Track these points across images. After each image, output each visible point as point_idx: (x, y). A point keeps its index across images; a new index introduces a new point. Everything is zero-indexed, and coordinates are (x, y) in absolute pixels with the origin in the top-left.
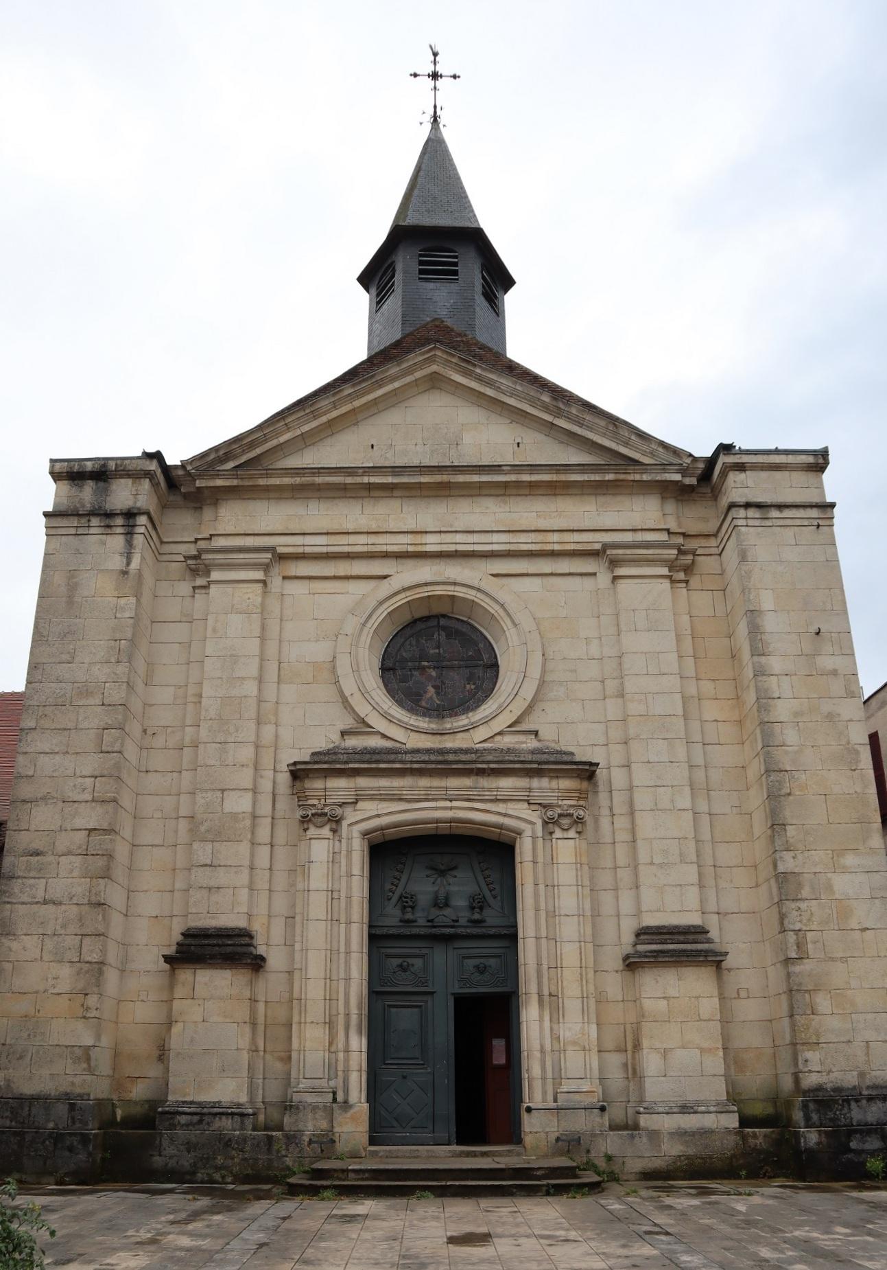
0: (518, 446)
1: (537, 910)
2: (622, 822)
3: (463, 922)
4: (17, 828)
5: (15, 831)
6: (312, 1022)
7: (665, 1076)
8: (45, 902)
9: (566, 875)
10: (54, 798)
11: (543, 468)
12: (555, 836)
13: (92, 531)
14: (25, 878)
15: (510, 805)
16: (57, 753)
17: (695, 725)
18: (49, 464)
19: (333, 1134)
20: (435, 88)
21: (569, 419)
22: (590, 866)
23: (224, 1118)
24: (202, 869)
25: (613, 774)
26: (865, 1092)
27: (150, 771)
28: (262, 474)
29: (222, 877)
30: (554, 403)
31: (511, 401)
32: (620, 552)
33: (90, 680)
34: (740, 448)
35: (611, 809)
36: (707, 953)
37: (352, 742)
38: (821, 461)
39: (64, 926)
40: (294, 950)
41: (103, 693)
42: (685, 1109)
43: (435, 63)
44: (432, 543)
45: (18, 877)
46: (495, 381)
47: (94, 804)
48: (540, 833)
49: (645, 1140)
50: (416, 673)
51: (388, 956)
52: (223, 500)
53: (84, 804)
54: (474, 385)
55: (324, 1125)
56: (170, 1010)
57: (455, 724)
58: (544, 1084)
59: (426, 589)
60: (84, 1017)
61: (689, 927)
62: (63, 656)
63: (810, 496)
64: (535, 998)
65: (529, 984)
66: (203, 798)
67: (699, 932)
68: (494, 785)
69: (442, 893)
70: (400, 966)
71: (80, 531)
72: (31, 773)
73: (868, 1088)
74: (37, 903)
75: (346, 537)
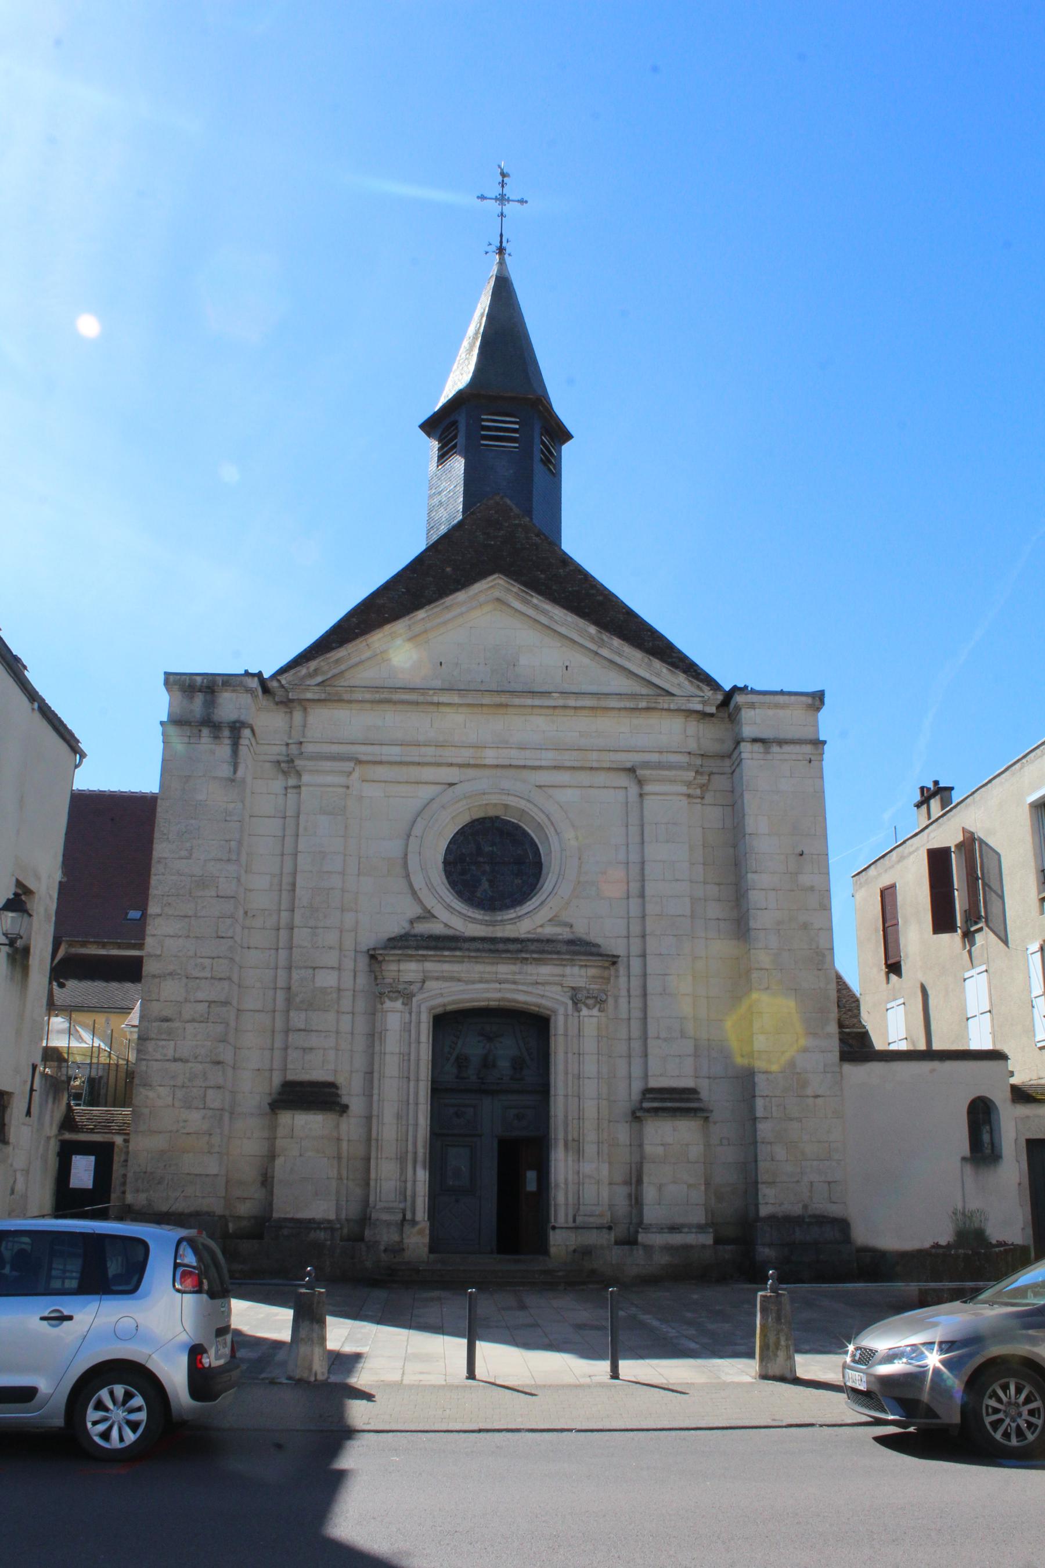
0: (567, 669)
1: (566, 1073)
6: (387, 1158)
8: (175, 1060)
10: (179, 974)
14: (157, 1039)
15: (547, 988)
16: (180, 936)
18: (163, 676)
26: (807, 1220)
29: (314, 1041)
30: (599, 635)
31: (562, 630)
34: (751, 688)
35: (629, 991)
38: (817, 703)
41: (217, 887)
43: (503, 184)
46: (548, 612)
47: (213, 981)
48: (570, 1012)
50: (473, 868)
53: (204, 980)
54: (531, 612)
55: (396, 1238)
58: (567, 1209)
63: (807, 733)
66: (298, 974)
67: (693, 1091)
72: (159, 953)
73: (810, 1216)
74: (168, 1060)
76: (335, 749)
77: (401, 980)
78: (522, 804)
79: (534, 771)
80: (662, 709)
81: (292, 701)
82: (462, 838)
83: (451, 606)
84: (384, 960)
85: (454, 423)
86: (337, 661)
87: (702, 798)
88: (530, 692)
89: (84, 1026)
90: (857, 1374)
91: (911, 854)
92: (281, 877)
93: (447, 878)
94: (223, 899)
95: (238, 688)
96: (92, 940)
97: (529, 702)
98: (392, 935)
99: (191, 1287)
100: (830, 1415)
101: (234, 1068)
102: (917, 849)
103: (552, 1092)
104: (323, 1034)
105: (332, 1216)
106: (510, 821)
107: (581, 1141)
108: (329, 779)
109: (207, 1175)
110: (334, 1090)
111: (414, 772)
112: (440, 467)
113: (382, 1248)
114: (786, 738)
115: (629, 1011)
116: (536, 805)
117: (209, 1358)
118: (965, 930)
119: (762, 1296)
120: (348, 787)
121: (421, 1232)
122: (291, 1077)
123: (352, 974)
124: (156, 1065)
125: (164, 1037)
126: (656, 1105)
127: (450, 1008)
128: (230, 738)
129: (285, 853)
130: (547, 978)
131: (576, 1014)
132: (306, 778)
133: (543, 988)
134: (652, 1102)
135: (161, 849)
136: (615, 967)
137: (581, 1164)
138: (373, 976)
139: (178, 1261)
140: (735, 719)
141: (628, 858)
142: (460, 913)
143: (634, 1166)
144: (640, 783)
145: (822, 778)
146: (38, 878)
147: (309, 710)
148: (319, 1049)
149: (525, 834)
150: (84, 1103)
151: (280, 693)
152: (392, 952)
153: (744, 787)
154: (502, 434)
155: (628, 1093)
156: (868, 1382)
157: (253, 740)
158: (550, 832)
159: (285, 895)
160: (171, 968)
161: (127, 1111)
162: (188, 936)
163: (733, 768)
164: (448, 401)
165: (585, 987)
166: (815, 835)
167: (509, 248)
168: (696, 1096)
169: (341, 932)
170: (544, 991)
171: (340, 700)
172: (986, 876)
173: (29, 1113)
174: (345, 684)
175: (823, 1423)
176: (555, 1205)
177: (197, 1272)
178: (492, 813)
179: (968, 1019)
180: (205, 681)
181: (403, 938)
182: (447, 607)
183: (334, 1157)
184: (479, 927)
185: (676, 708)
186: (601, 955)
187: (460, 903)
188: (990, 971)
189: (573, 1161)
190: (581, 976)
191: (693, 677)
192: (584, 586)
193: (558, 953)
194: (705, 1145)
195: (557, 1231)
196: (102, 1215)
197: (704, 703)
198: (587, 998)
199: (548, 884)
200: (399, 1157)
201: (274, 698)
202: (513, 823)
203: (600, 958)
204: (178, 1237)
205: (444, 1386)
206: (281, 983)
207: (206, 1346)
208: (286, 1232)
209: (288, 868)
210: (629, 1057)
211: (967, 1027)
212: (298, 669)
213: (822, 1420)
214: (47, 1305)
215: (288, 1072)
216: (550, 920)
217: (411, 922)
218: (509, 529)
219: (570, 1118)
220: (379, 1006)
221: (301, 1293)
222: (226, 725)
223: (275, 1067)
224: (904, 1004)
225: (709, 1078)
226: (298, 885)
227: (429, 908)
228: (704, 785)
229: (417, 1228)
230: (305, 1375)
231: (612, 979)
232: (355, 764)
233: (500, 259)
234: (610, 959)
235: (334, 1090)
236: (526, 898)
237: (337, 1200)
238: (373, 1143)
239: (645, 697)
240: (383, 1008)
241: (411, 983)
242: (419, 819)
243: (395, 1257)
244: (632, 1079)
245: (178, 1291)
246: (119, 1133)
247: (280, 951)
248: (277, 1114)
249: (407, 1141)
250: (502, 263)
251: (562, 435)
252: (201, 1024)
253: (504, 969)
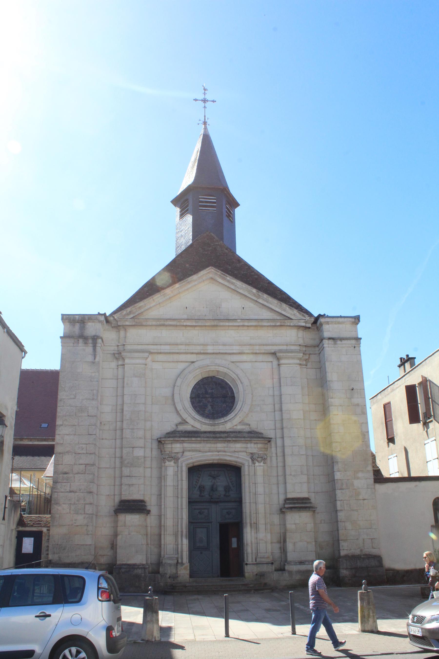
0: (243, 309)
1: (250, 492)
4: (58, 464)
5: (57, 464)
6: (169, 534)
7: (294, 551)
8: (70, 492)
10: (71, 452)
11: (253, 320)
14: (62, 482)
15: (240, 453)
16: (72, 435)
19: (177, 574)
20: (205, 107)
26: (362, 557)
27: (104, 439)
28: (144, 321)
31: (241, 291)
33: (82, 406)
34: (327, 315)
35: (276, 454)
36: (309, 507)
38: (357, 321)
39: (78, 501)
41: (88, 411)
43: (205, 94)
45: (59, 482)
47: (87, 455)
50: (204, 400)
51: (195, 509)
55: (174, 571)
63: (353, 335)
64: (249, 525)
67: (308, 499)
72: (62, 442)
73: (364, 555)
74: (67, 492)
76: (140, 347)
77: (173, 452)
78: (225, 370)
79: (230, 355)
80: (287, 326)
81: (119, 326)
82: (198, 386)
83: (191, 281)
84: (165, 443)
85: (187, 200)
86: (140, 308)
87: (306, 365)
88: (227, 319)
89: (25, 477)
90: (416, 628)
91: (397, 388)
92: (117, 406)
93: (192, 405)
94: (91, 417)
95: (95, 321)
96: (26, 437)
97: (227, 324)
98: (168, 432)
99: (105, 598)
100: (399, 649)
101: (97, 495)
102: (400, 386)
103: (243, 501)
104: (138, 478)
105: (144, 562)
106: (220, 378)
107: (257, 523)
108: (137, 361)
109: (86, 545)
110: (144, 503)
111: (176, 357)
112: (181, 220)
113: (168, 576)
114: (343, 337)
115: (277, 463)
116: (231, 370)
117: (115, 632)
118: (424, 421)
119: (360, 593)
120: (146, 365)
121: (185, 568)
122: (124, 498)
124: (61, 494)
125: (65, 481)
126: (291, 506)
127: (196, 464)
128: (92, 343)
129: (118, 395)
130: (240, 449)
131: (253, 465)
132: (127, 361)
133: (238, 454)
134: (289, 504)
135: (62, 395)
136: (270, 443)
137: (258, 534)
138: (160, 450)
139: (99, 586)
140: (320, 329)
141: (274, 393)
142: (198, 420)
143: (282, 534)
144: (278, 359)
145: (360, 355)
146: (7, 409)
147: (127, 330)
148: (136, 485)
149: (227, 384)
150: (27, 513)
151: (114, 323)
152: (169, 439)
153: (326, 360)
154: (209, 204)
156: (422, 632)
157: (102, 344)
158: (238, 382)
159: (119, 414)
161: (48, 516)
162: (75, 435)
163: (320, 351)
164: (183, 191)
165: (257, 453)
166: (358, 380)
167: (208, 122)
168: (309, 501)
169: (145, 430)
170: (238, 455)
171: (142, 325)
172: (433, 397)
173: (4, 519)
174: (144, 318)
175: (397, 652)
176: (247, 554)
177: (108, 591)
178: (211, 375)
179: (427, 462)
180: (80, 318)
181: (174, 433)
182: (188, 282)
183: (145, 535)
184: (207, 426)
185: (293, 325)
186: (262, 438)
187: (198, 416)
188: (437, 440)
189: (254, 533)
190: (255, 448)
191: (299, 310)
192: (249, 271)
193: (244, 437)
194: (314, 524)
195: (248, 565)
196: (38, 566)
197: (306, 322)
198: (258, 457)
199: (238, 406)
200: (174, 533)
201: (111, 325)
202: (221, 379)
203: (263, 439)
204: (99, 575)
205: (214, 641)
206: (118, 455)
207: (113, 626)
208: (123, 570)
209: (120, 402)
210: (278, 484)
211: (427, 466)
212: (123, 311)
213: (396, 651)
214: (38, 610)
215: (122, 496)
216: (240, 423)
217: (177, 425)
218: (214, 247)
219: (252, 513)
220: (163, 464)
221: (147, 599)
222: (90, 337)
224: (397, 456)
225: (314, 492)
226: (124, 410)
227: (185, 419)
228: (307, 360)
229: (184, 566)
230: (150, 638)
231: (269, 448)
232: (149, 354)
233: (204, 127)
234: (267, 440)
235: (144, 503)
236: (228, 413)
237: (146, 555)
238: (162, 528)
239: (279, 320)
240: (165, 465)
241: (177, 453)
242: (179, 378)
243: (174, 580)
244: (279, 494)
245: (100, 600)
246: (45, 526)
247: (117, 440)
248: (117, 515)
249: (178, 526)
250: (206, 128)
251: (236, 204)
252: (82, 475)
253: (220, 446)
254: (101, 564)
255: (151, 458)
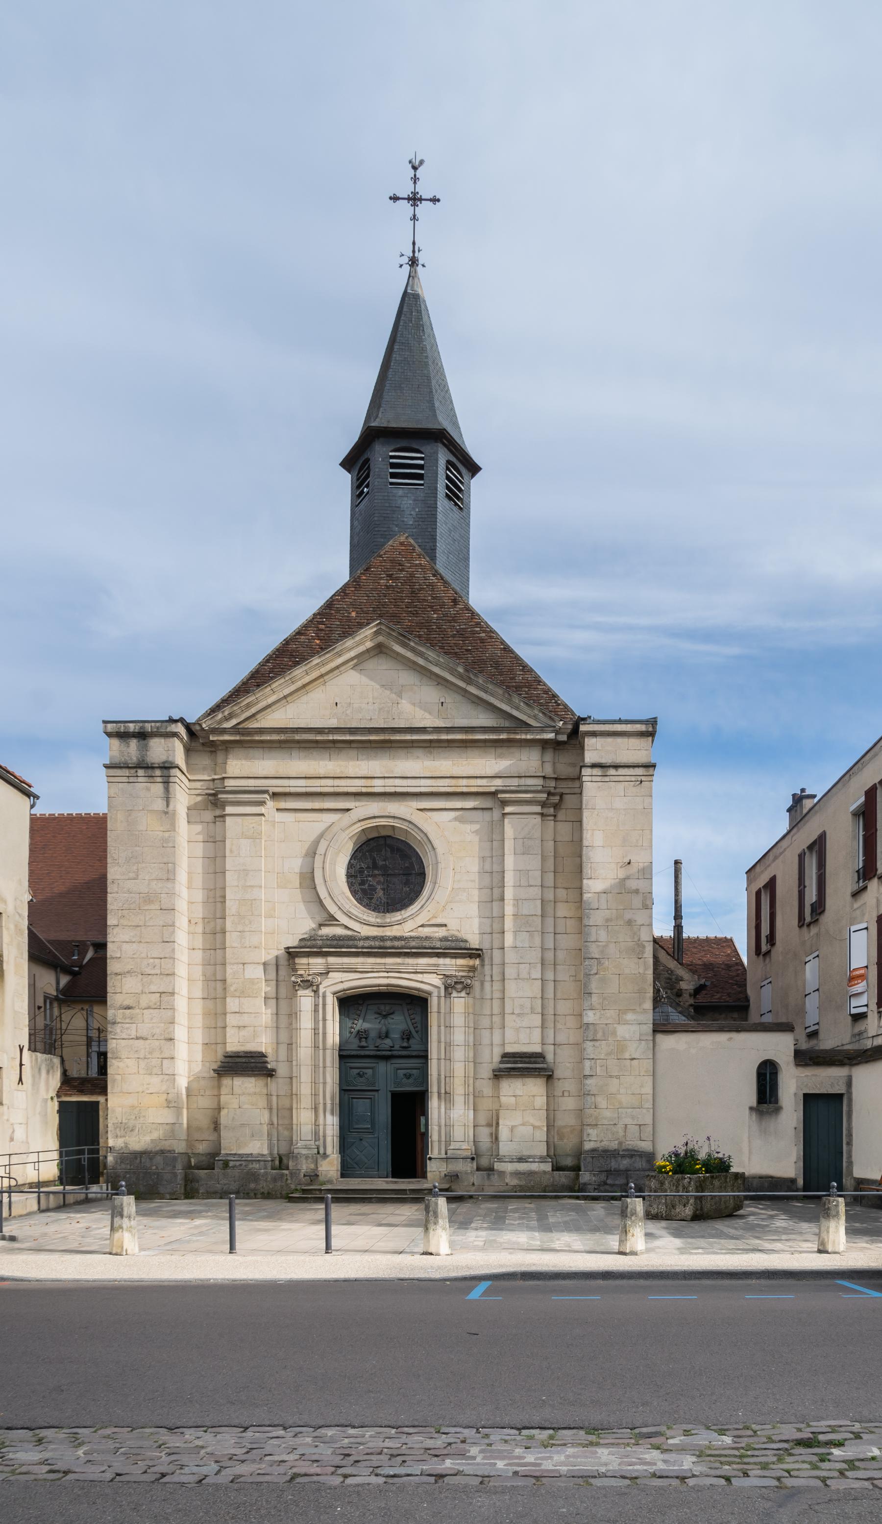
1: (439, 1042)
2: (497, 986)
3: (397, 1047)
8: (137, 1038)
9: (458, 1020)
12: (452, 995)
13: (140, 779)
17: (550, 921)
20: (414, 216)
21: (479, 687)
22: (474, 1014)
23: (254, 1163)
24: (234, 1015)
25: (494, 954)
31: (436, 670)
32: (507, 795)
37: (326, 931)
40: (292, 1065)
42: (521, 1160)
43: (415, 180)
44: (378, 786)
45: (118, 1023)
48: (443, 994)
49: (496, 1176)
51: (351, 1068)
52: (231, 748)
55: (312, 1166)
56: (219, 1101)
57: (393, 919)
59: (374, 820)
60: (168, 1107)
61: (533, 1053)
62: (130, 874)
65: (433, 1088)
67: (539, 1057)
68: (415, 962)
69: (384, 1030)
70: (359, 1074)
71: (132, 780)
73: (623, 1150)
74: (132, 1039)
75: (319, 780)
123: (274, 967)
125: (127, 1021)
155: (491, 1058)
158: (428, 848)
160: (128, 967)
167: (421, 257)
197: (557, 733)
223: (489, 1002)
250: (412, 276)
254: (199, 1154)
255: (277, 981)
